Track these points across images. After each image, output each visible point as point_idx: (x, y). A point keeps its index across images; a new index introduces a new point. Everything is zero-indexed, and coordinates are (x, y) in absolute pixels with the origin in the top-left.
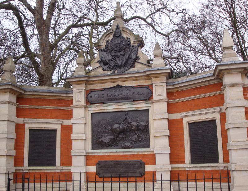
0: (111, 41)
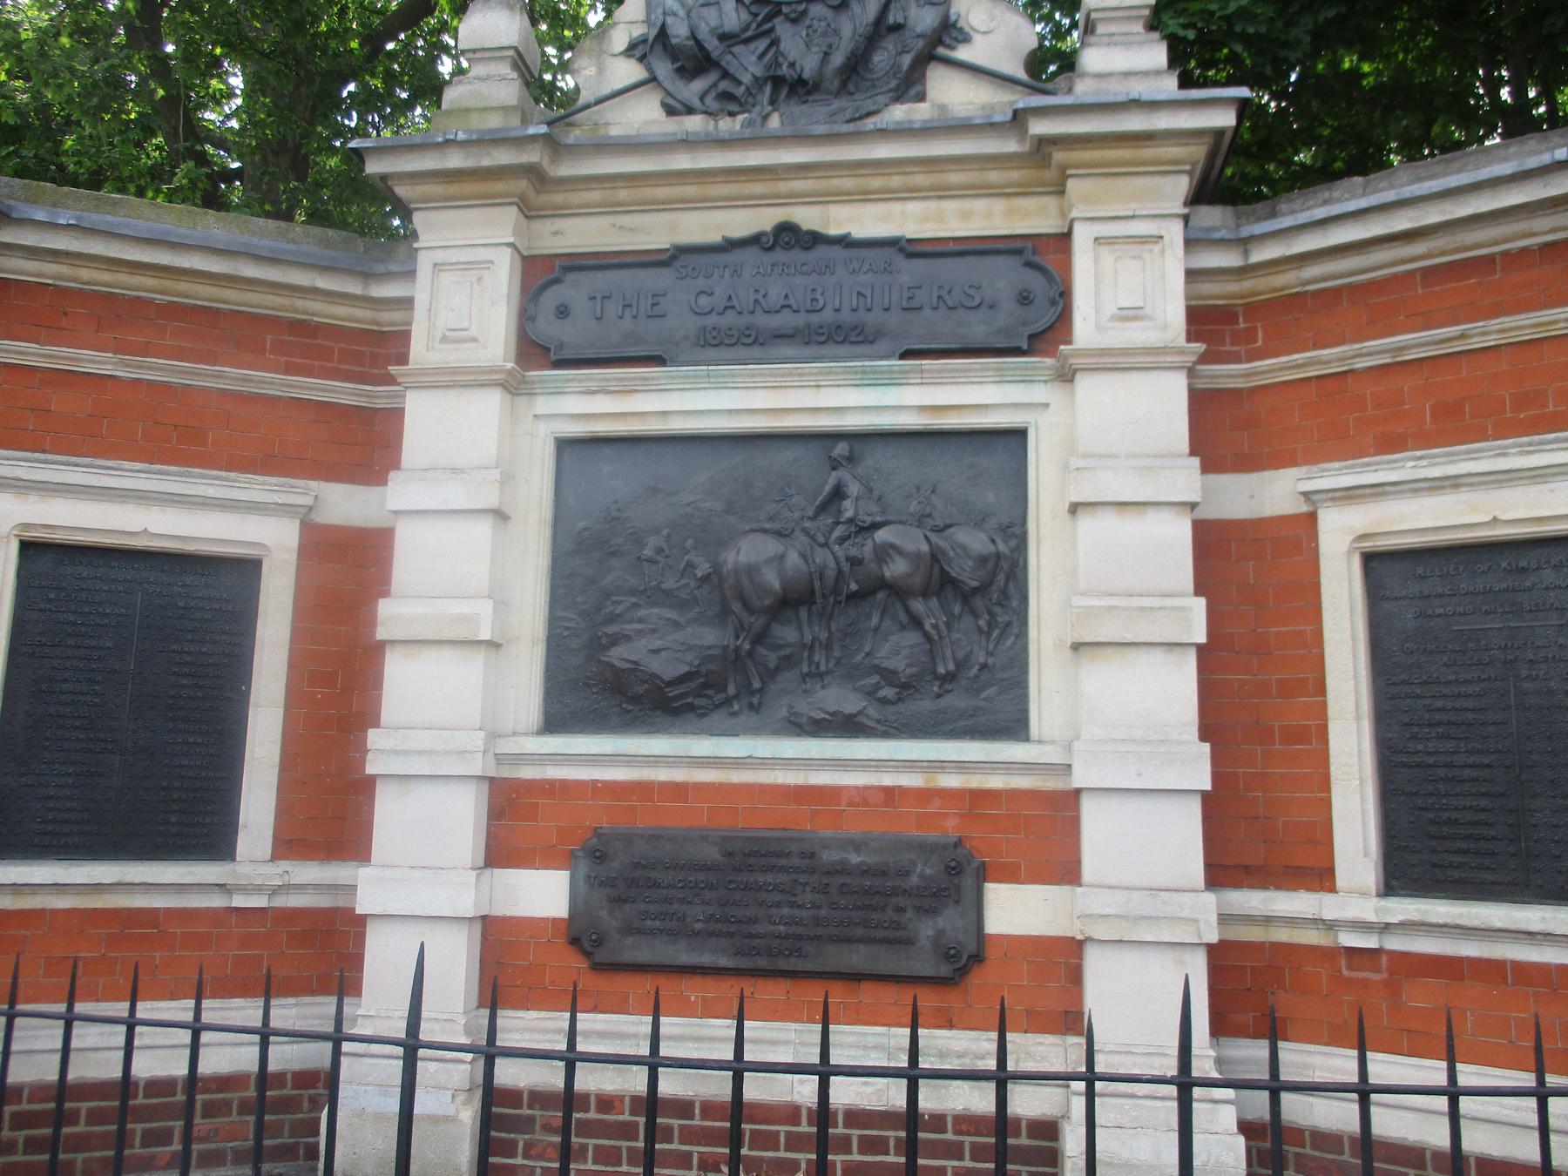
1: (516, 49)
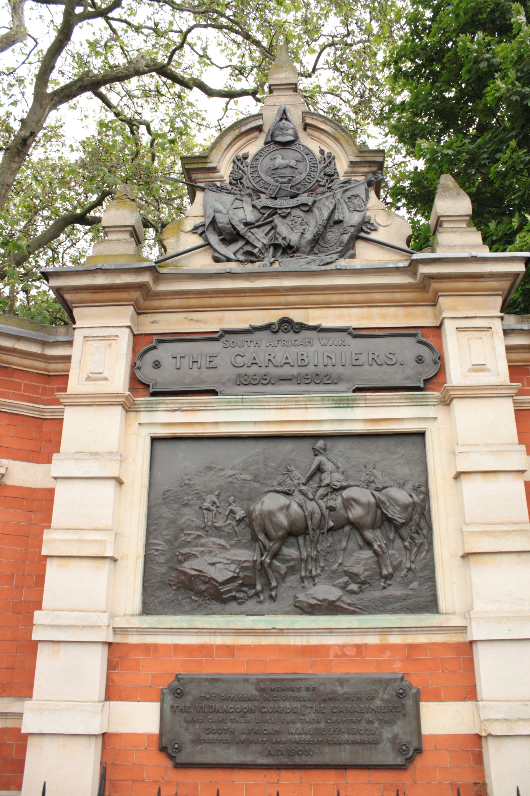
0: (256, 158)
1: (133, 227)
